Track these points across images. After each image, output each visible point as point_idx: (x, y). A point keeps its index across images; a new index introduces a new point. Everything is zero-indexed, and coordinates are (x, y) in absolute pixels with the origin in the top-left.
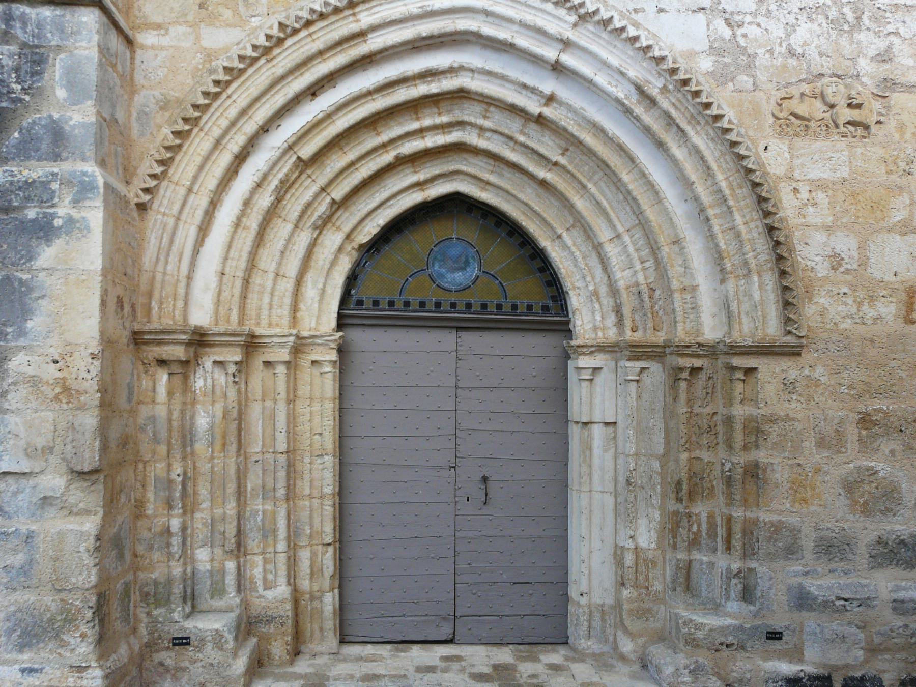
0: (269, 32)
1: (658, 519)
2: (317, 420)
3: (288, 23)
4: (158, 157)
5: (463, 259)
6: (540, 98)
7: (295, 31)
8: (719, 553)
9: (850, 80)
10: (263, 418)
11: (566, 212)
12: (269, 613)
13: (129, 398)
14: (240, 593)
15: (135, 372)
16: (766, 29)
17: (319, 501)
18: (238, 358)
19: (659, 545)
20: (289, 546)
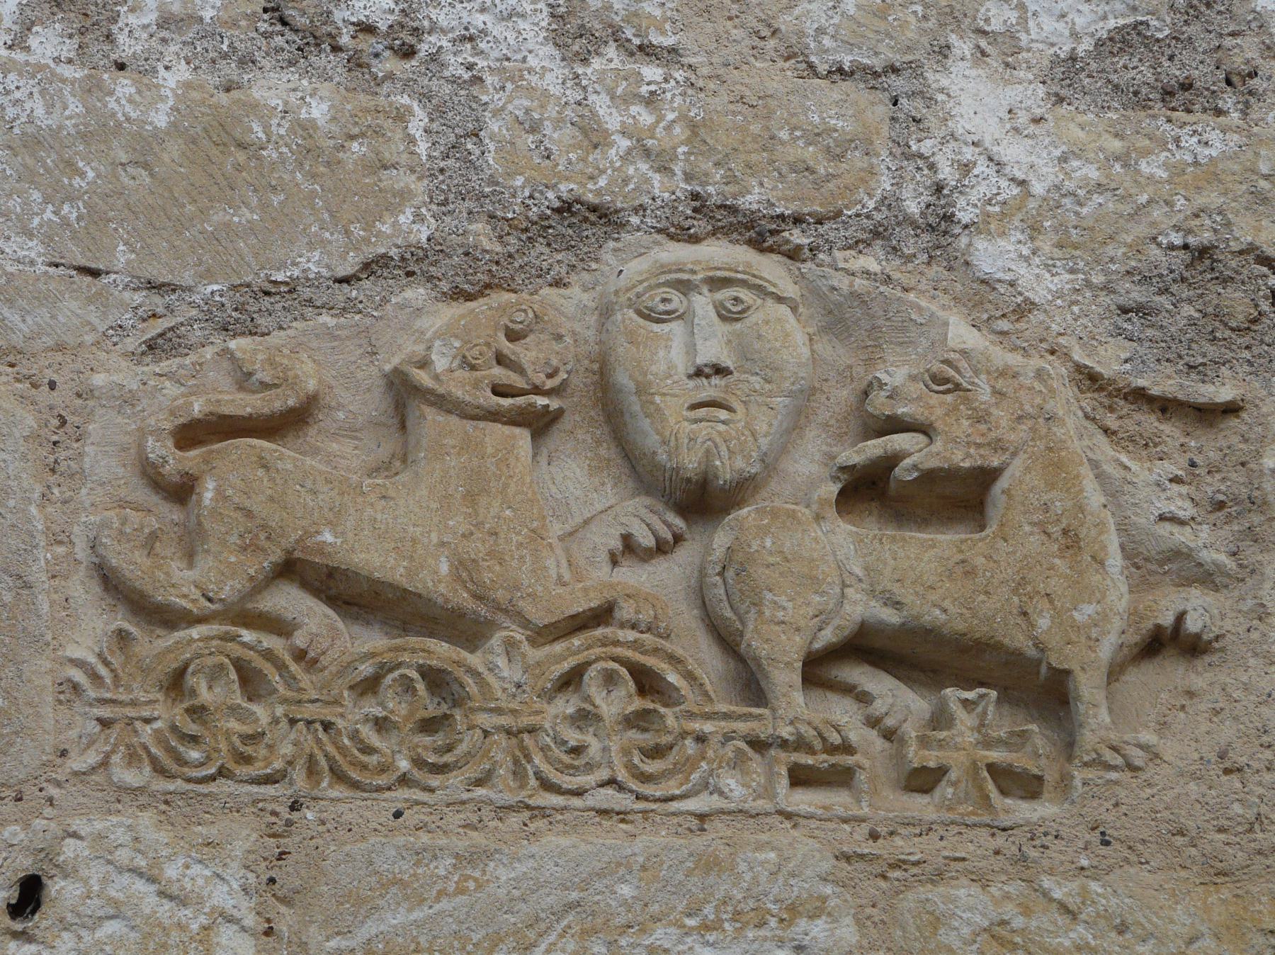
9: (869, 262)
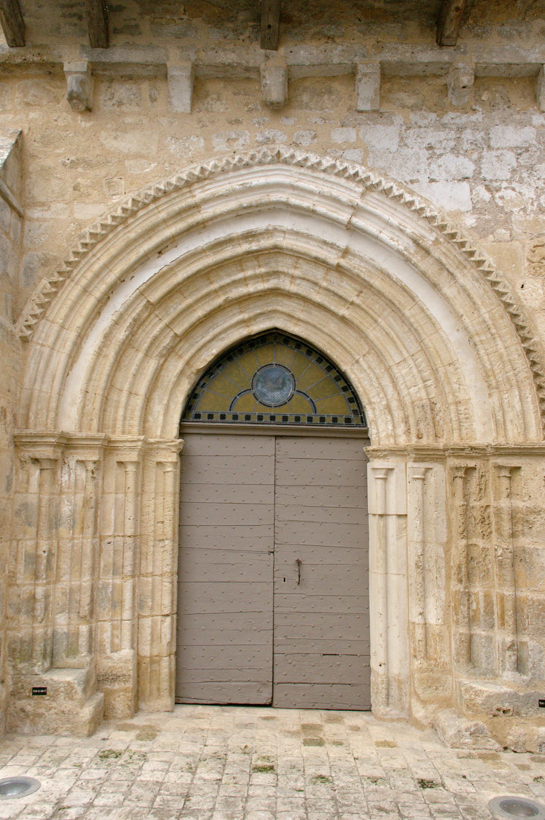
0: (125, 206)
1: (444, 598)
2: (160, 511)
3: (139, 199)
4: (38, 301)
5: (281, 381)
6: (338, 252)
7: (145, 205)
8: (496, 628)
10: (115, 508)
11: (363, 342)
12: (114, 672)
13: (7, 487)
14: (91, 654)
15: (14, 468)
16: (520, 193)
17: (160, 578)
18: (95, 458)
19: (446, 622)
20: (133, 615)
